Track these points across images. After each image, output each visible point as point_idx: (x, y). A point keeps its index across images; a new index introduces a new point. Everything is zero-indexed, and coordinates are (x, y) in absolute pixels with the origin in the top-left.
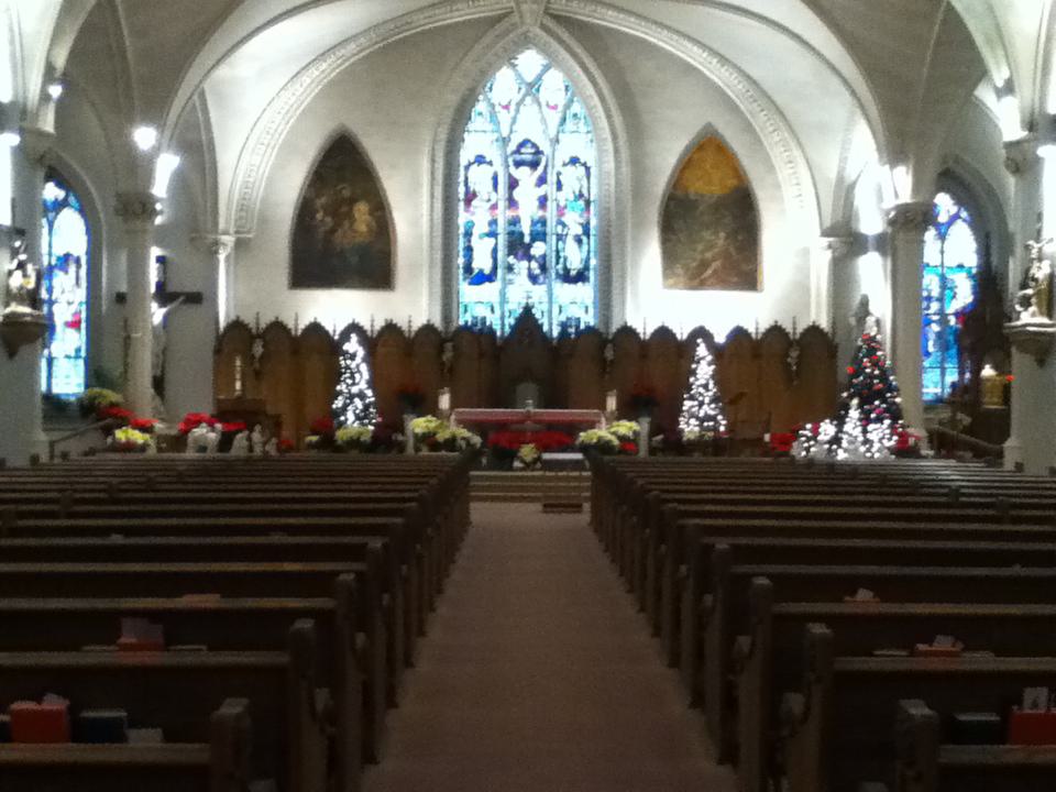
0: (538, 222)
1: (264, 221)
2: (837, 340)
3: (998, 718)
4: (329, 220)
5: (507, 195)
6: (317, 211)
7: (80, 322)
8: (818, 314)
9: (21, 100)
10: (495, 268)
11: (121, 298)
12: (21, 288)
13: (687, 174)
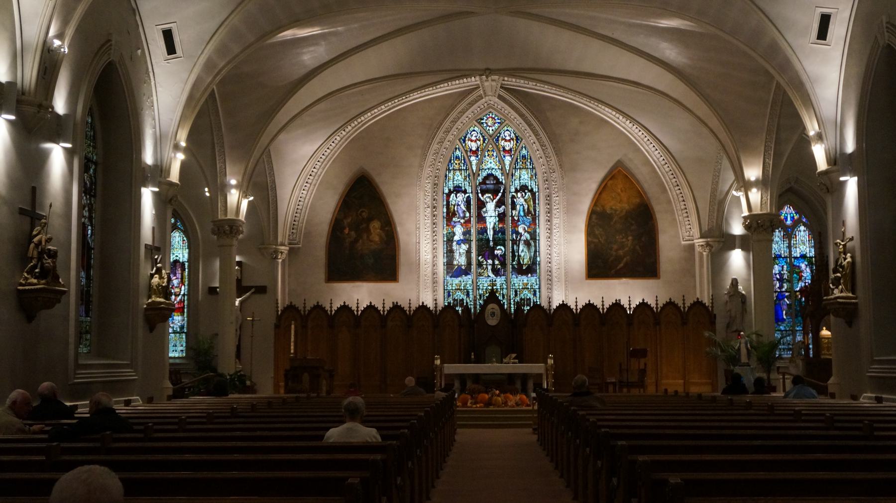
0: (499, 231)
1: (308, 234)
2: (715, 312)
3: (473, 319)
4: (353, 233)
5: (237, 343)
6: (345, 228)
7: (183, 307)
8: (702, 292)
9: (159, 163)
10: (469, 264)
11: (212, 291)
12: (159, 285)
13: (604, 195)
